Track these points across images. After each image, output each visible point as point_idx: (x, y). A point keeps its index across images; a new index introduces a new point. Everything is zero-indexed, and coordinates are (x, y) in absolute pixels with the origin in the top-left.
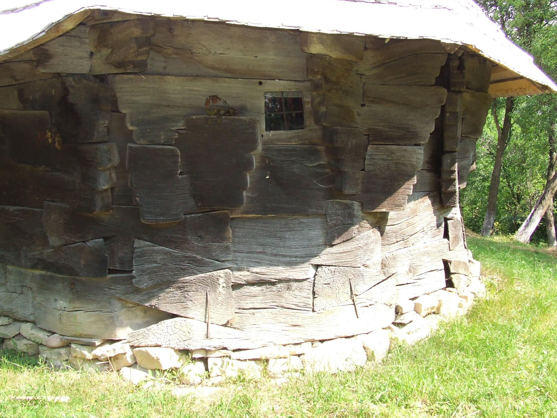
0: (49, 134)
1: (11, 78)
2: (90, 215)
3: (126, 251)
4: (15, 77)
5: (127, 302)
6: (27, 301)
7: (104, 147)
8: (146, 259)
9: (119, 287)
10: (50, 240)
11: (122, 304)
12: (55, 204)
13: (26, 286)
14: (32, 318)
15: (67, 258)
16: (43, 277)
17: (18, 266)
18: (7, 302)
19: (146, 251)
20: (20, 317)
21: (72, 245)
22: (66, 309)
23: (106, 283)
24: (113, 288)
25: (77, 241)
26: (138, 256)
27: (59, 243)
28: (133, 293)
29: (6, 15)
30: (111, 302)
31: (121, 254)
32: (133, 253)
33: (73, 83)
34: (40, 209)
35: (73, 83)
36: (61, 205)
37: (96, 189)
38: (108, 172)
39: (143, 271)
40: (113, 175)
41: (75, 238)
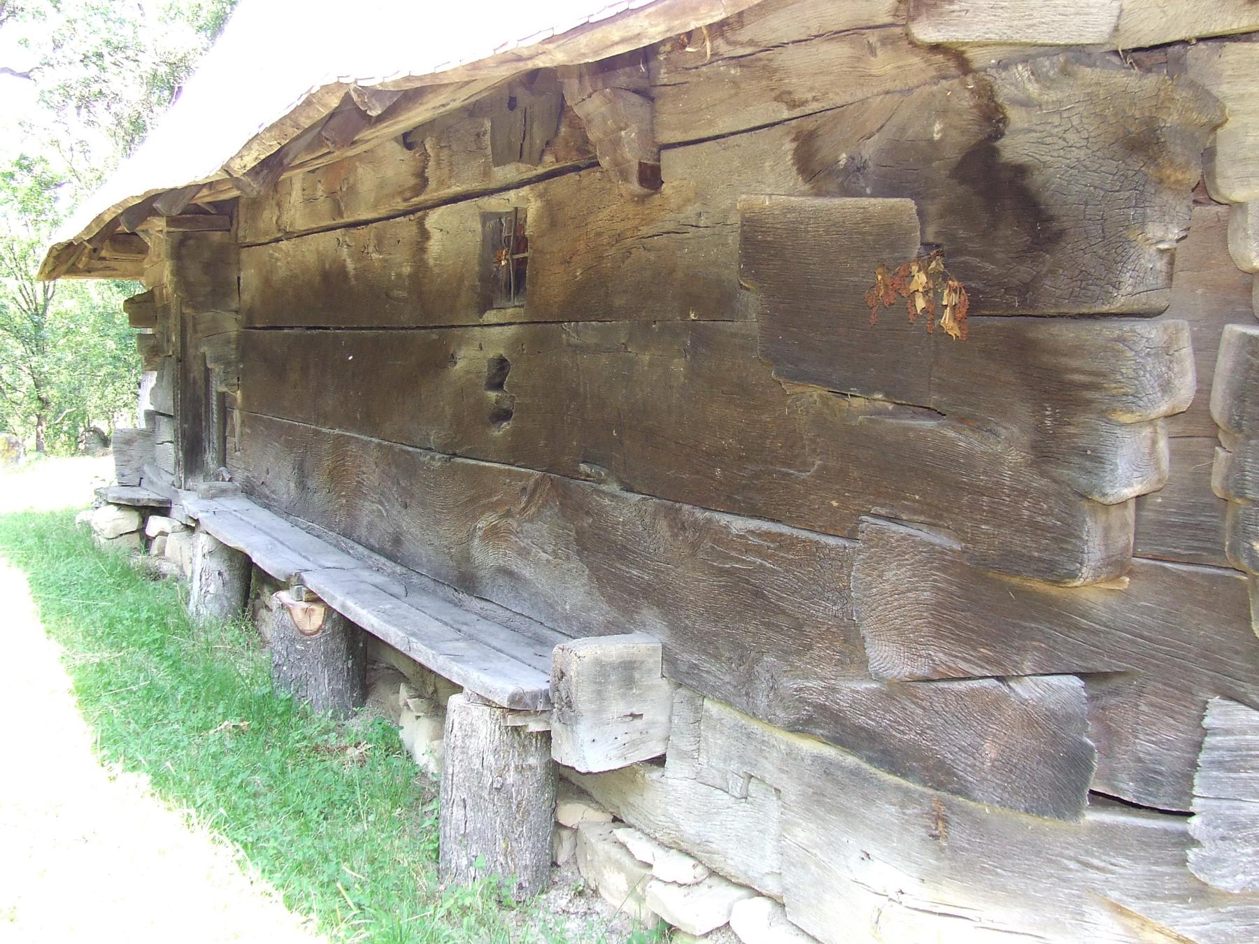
0: (920, 279)
1: (776, 99)
2: (1054, 591)
3: (1167, 735)
4: (790, 93)
5: (1144, 923)
6: (761, 827)
7: (1150, 332)
8: (1252, 779)
10: (871, 652)
11: (1128, 929)
12: (902, 529)
13: (762, 781)
14: (772, 886)
15: (929, 728)
16: (827, 769)
17: (743, 712)
18: (696, 812)
19: (1251, 750)
20: (733, 872)
21: (956, 686)
22: (902, 897)
23: (1071, 840)
24: (1096, 862)
25: (977, 672)
26: (1220, 764)
27: (907, 670)
28: (1182, 899)
29: (228, 852)
30: (1082, 914)
31: (1144, 746)
32: (1199, 746)
33: (1033, 89)
34: (841, 542)
35: (1033, 89)
36: (924, 535)
37: (1096, 497)
38: (1147, 431)
39: (1235, 825)
40: (1163, 445)
41: (964, 659)
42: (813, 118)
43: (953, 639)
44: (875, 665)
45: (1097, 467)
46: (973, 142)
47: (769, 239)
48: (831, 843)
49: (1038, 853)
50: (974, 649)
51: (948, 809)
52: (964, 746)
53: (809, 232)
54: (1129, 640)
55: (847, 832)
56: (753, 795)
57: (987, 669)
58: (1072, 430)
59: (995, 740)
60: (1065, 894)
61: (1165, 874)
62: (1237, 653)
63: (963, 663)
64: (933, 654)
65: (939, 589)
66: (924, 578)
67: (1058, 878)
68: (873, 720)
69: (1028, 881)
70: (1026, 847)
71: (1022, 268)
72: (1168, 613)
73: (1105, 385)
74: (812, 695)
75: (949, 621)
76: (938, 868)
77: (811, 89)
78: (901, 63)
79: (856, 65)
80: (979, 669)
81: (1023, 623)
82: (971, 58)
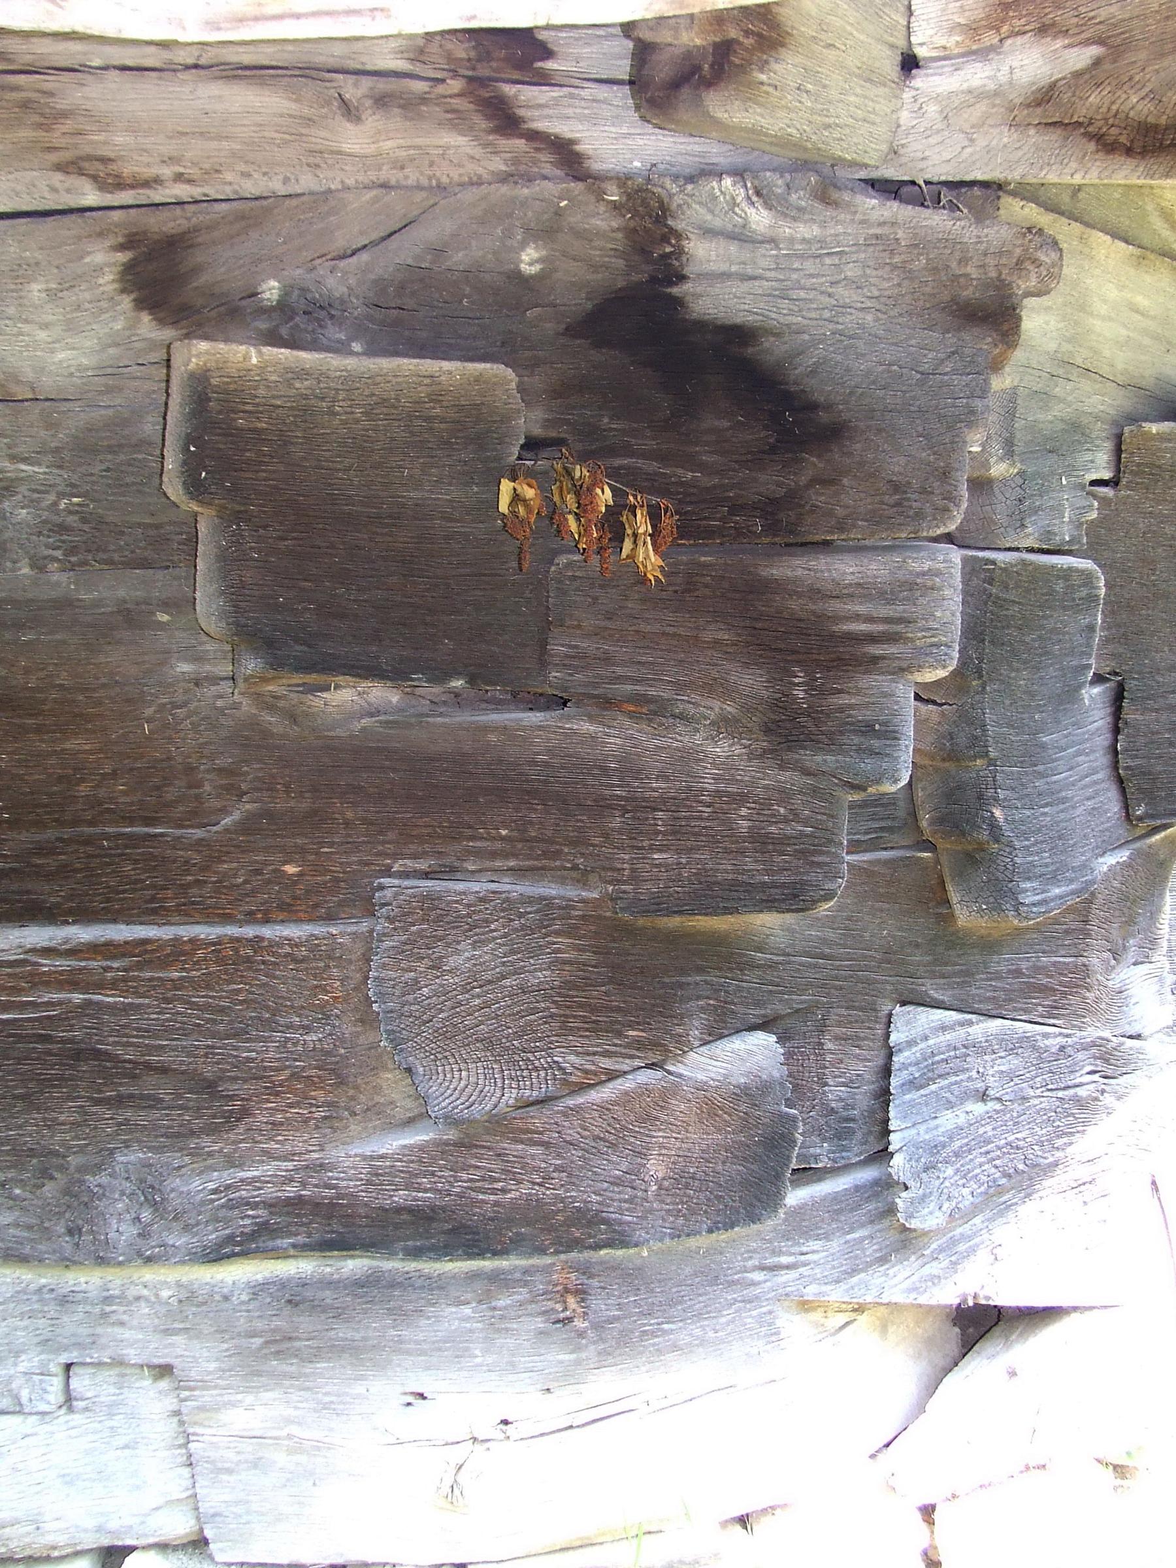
9: (813, 1252)
21: (594, 1096)
24: (785, 1260)
26: (913, 1084)
39: (935, 1148)
42: (164, 214)
43: (587, 1030)
44: (443, 1104)
45: (890, 746)
46: (620, 284)
47: (259, 425)
48: (326, 1406)
49: (715, 1281)
50: (619, 1034)
51: (584, 1273)
52: (618, 1178)
53: (338, 414)
54: (810, 965)
55: (362, 1378)
56: (89, 1395)
57: (639, 1057)
58: (844, 700)
59: (663, 1152)
60: (753, 1317)
61: (863, 1239)
62: (917, 946)
63: (606, 1060)
64: (560, 1060)
65: (565, 962)
66: (533, 952)
67: (743, 1301)
68: (426, 1191)
69: (706, 1323)
70: (697, 1280)
71: (762, 477)
72: (849, 919)
73: (910, 635)
74: (260, 1189)
75: (581, 1006)
76: (578, 1363)
77: (172, 160)
78: (419, 141)
79: (303, 131)
80: (627, 1061)
81: (684, 980)
82: (590, 152)
